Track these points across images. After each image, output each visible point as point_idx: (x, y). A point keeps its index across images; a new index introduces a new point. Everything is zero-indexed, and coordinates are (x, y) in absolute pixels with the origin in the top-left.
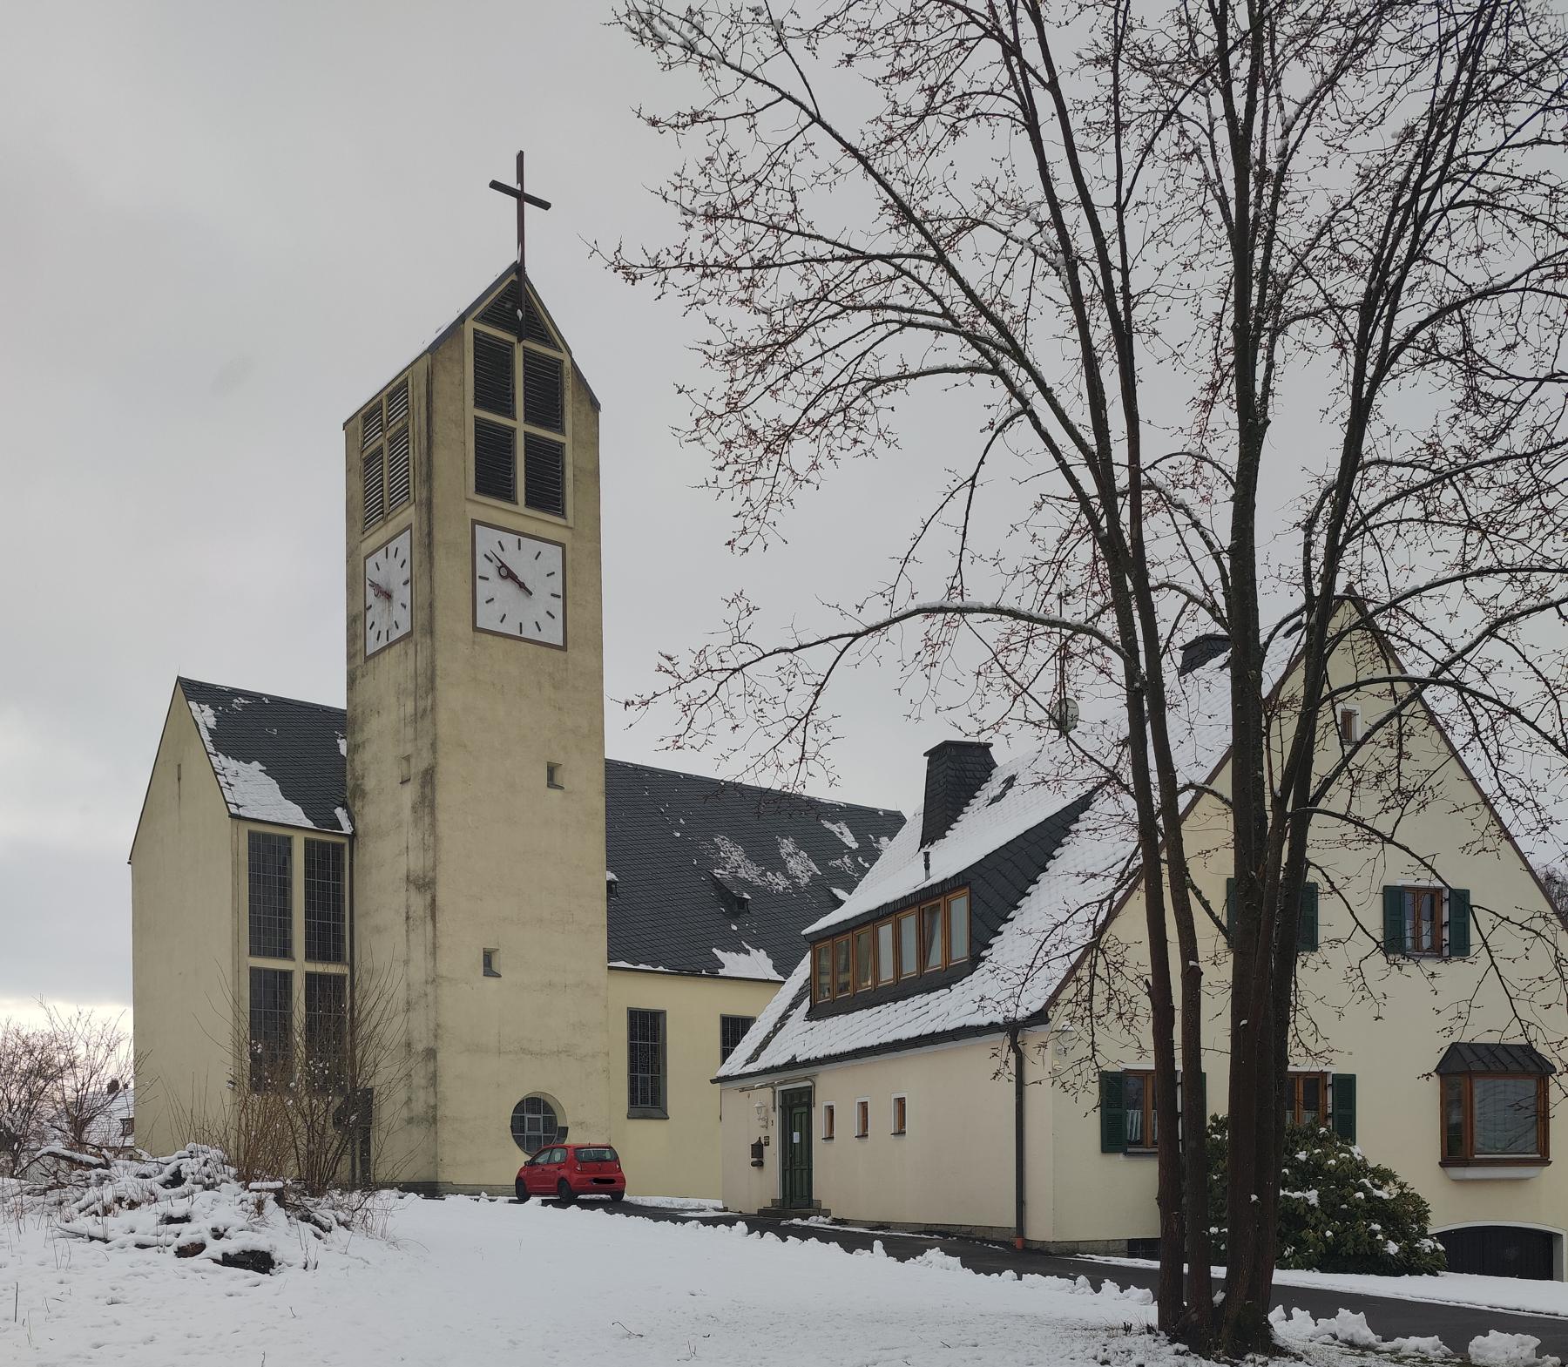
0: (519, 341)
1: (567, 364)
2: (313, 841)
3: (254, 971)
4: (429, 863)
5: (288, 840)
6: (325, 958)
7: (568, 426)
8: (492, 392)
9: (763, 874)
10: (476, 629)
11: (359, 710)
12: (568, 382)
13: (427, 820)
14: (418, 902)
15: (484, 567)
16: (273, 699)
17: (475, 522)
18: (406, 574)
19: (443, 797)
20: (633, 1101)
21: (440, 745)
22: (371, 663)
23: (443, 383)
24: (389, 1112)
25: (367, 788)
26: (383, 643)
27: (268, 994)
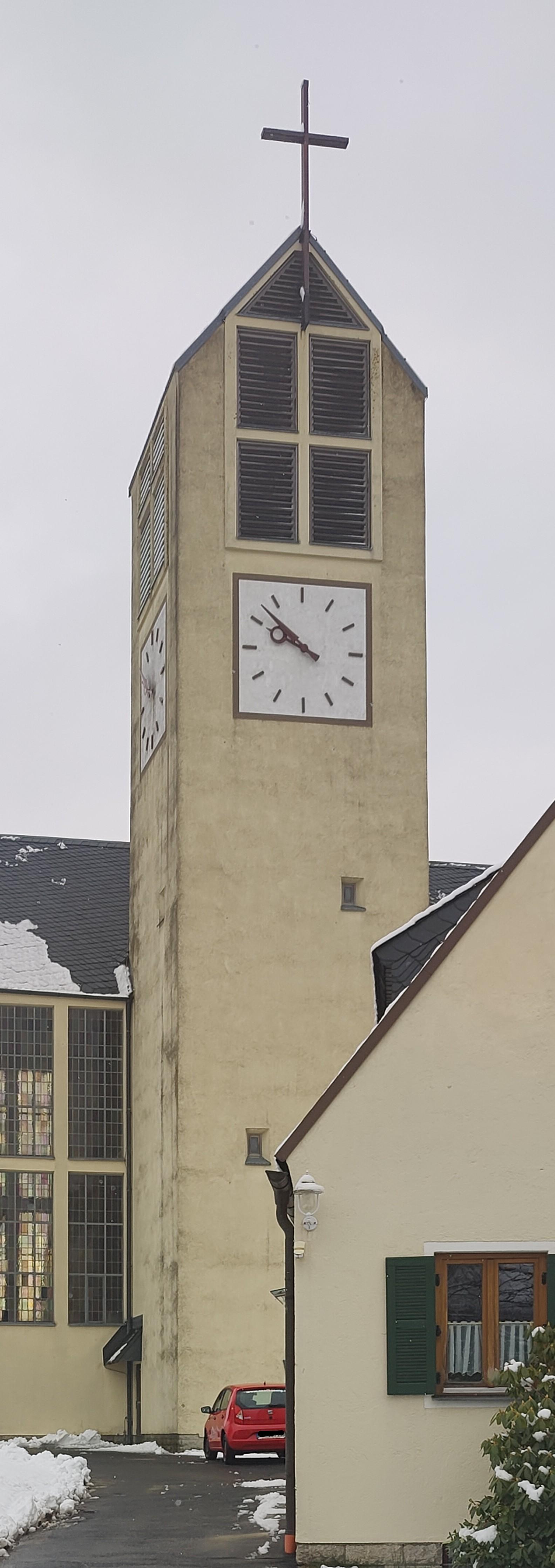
0: (303, 329)
1: (376, 343)
2: (81, 1010)
5: (48, 1012)
6: (96, 1154)
7: (376, 426)
10: (237, 714)
12: (376, 368)
15: (249, 632)
16: (72, 844)
17: (237, 577)
20: (69, 1322)
24: (152, 1346)
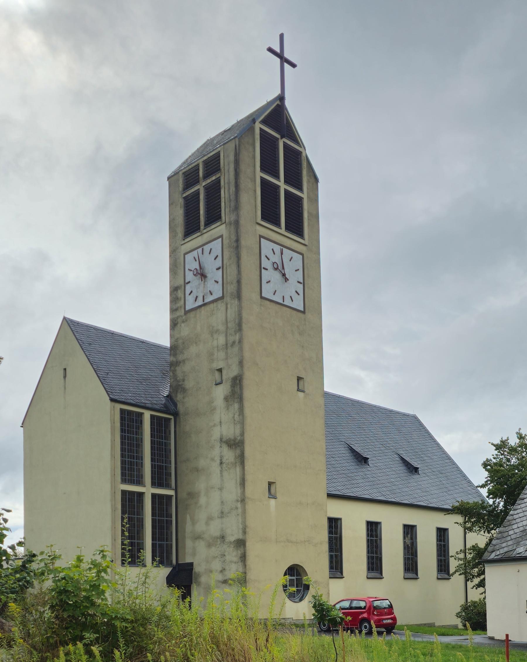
1: (304, 154)
3: (124, 492)
4: (238, 431)
8: (269, 164)
11: (180, 341)
13: (236, 406)
14: (229, 455)
17: (261, 237)
18: (219, 263)
19: (248, 394)
21: (245, 362)
22: (188, 315)
23: (245, 156)
25: (187, 387)
26: (200, 302)
27: (131, 504)
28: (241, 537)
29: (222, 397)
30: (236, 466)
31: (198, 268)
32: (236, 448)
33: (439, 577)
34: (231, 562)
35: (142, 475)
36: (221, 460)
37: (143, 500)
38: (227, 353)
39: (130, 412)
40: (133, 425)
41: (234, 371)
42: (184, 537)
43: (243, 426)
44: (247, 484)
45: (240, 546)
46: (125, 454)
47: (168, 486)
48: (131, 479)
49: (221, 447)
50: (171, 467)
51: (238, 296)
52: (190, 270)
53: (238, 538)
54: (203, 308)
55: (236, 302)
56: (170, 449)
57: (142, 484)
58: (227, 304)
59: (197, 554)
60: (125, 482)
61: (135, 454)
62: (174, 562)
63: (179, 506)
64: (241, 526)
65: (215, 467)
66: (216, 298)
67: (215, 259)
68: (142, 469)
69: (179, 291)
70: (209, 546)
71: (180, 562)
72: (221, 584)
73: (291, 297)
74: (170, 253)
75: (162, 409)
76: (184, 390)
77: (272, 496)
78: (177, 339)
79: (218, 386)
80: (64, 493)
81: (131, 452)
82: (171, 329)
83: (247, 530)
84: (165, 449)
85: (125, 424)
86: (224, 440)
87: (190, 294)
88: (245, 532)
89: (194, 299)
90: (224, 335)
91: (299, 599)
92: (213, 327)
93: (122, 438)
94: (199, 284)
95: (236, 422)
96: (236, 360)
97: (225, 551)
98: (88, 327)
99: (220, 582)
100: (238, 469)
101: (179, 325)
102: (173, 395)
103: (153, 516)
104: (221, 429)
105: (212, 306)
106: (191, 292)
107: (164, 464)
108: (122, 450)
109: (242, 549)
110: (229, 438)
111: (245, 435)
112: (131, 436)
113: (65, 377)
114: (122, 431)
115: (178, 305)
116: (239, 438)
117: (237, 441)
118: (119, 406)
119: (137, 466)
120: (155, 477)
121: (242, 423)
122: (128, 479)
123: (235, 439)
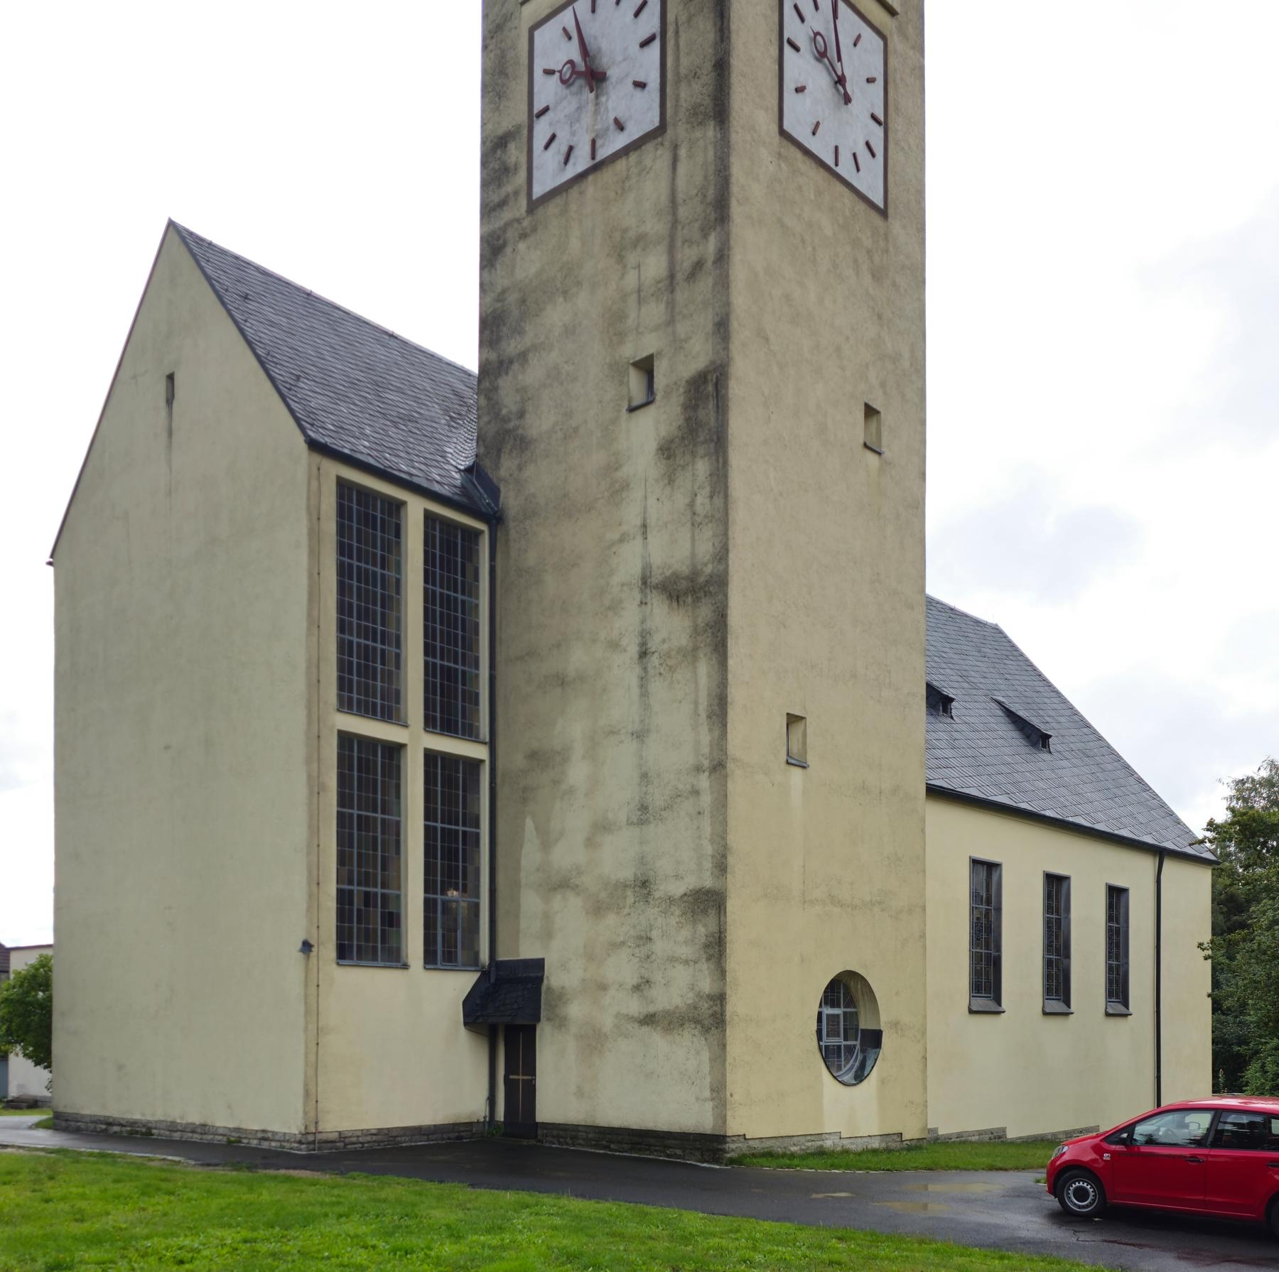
3: (346, 739)
4: (705, 548)
9: (73, 1206)
11: (512, 298)
13: (702, 467)
14: (671, 626)
19: (745, 425)
21: (734, 325)
22: (540, 211)
25: (533, 432)
26: (581, 162)
27: (365, 774)
28: (708, 882)
29: (651, 445)
30: (695, 659)
31: (577, 58)
32: (697, 600)
33: (1111, 1011)
34: (673, 960)
35: (398, 692)
36: (643, 644)
37: (399, 768)
38: (671, 305)
39: (366, 495)
40: (375, 536)
41: (698, 356)
42: (516, 884)
43: (726, 530)
44: (733, 714)
45: (705, 912)
46: (351, 623)
47: (469, 733)
48: (367, 702)
49: (643, 603)
50: (477, 676)
51: (719, 109)
52: (549, 72)
53: (699, 886)
54: (591, 178)
55: (711, 131)
56: (477, 625)
57: (398, 719)
58: (675, 148)
59: (554, 933)
60: (350, 707)
61: (379, 628)
62: (484, 956)
63: (502, 793)
64: (709, 849)
65: (623, 670)
66: (636, 137)
67: (637, 14)
68: (398, 675)
69: (512, 147)
70: (597, 910)
71: (502, 956)
72: (636, 1025)
73: (854, 155)
74: (484, 39)
75: (456, 497)
76: (523, 444)
77: (796, 761)
78: (504, 292)
79: (638, 412)
80: (167, 748)
81: (367, 620)
82: (482, 268)
83: (731, 860)
84: (464, 621)
85: (351, 528)
86: (656, 579)
87: (547, 147)
88: (721, 867)
89: (562, 158)
90: (662, 248)
91: (852, 1074)
92: (625, 231)
93: (343, 571)
94: (579, 109)
95: (698, 519)
96: (705, 321)
97: (651, 927)
98: (241, 264)
99: (631, 1019)
100: (704, 669)
101: (508, 250)
102: (487, 464)
103: (427, 818)
104: (645, 546)
105: (621, 165)
106: (553, 137)
107: (460, 667)
108: (343, 608)
109: (711, 922)
110: (674, 574)
111: (732, 555)
112: (367, 570)
113: (170, 400)
114: (343, 549)
115: (509, 188)
116: (708, 569)
117: (701, 580)
118: (334, 470)
119: (383, 663)
120: (434, 701)
121: (722, 519)
122: (359, 701)
123: (694, 575)
